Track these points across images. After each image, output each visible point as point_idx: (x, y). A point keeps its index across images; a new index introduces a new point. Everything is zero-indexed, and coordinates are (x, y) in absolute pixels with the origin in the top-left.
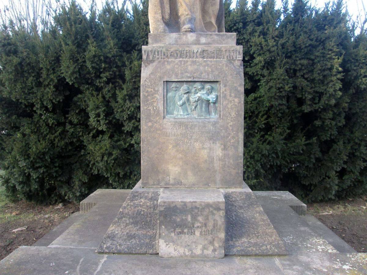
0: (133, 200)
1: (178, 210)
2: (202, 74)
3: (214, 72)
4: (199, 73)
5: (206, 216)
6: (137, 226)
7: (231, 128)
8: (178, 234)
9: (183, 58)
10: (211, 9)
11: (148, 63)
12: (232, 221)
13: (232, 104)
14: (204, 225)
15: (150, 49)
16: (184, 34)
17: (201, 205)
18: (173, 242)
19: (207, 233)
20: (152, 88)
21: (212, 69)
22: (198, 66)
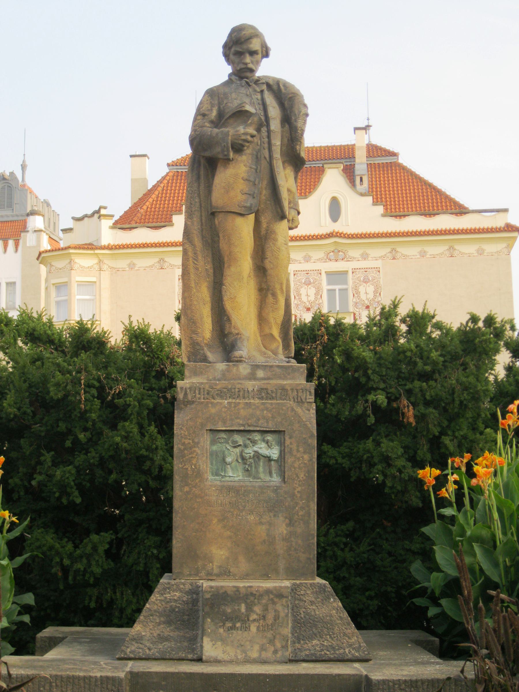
1: (228, 598)
2: (259, 420)
4: (255, 419)
7: (299, 495)
8: (229, 630)
10: (271, 316)
11: (184, 405)
12: (299, 620)
15: (188, 386)
16: (234, 365)
20: (189, 439)
21: (272, 414)
22: (253, 409)
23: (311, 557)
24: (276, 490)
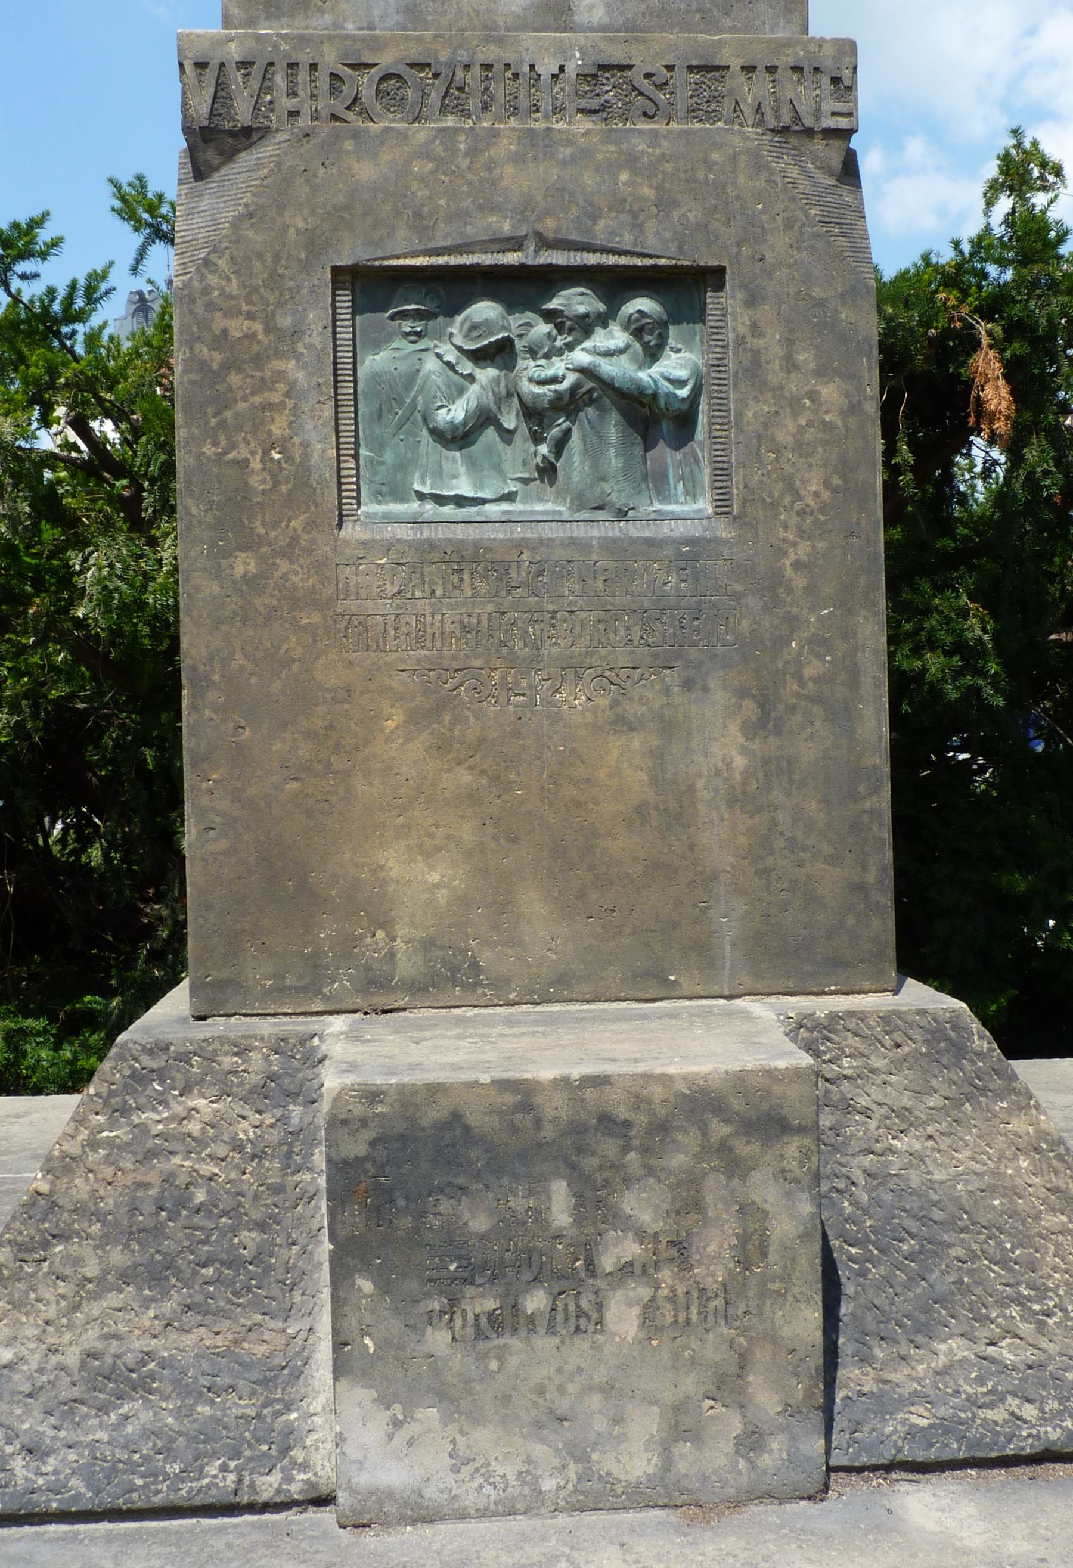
0: (124, 1111)
2: (594, 217)
3: (675, 204)
4: (574, 212)
5: (679, 1185)
6: (166, 1294)
8: (480, 1334)
9: (466, 114)
13: (803, 422)
14: (673, 1253)
17: (639, 1102)
18: (442, 1395)
19: (694, 1310)
20: (251, 316)
21: (659, 188)
22: (564, 163)
23: (871, 878)
24: (693, 558)
